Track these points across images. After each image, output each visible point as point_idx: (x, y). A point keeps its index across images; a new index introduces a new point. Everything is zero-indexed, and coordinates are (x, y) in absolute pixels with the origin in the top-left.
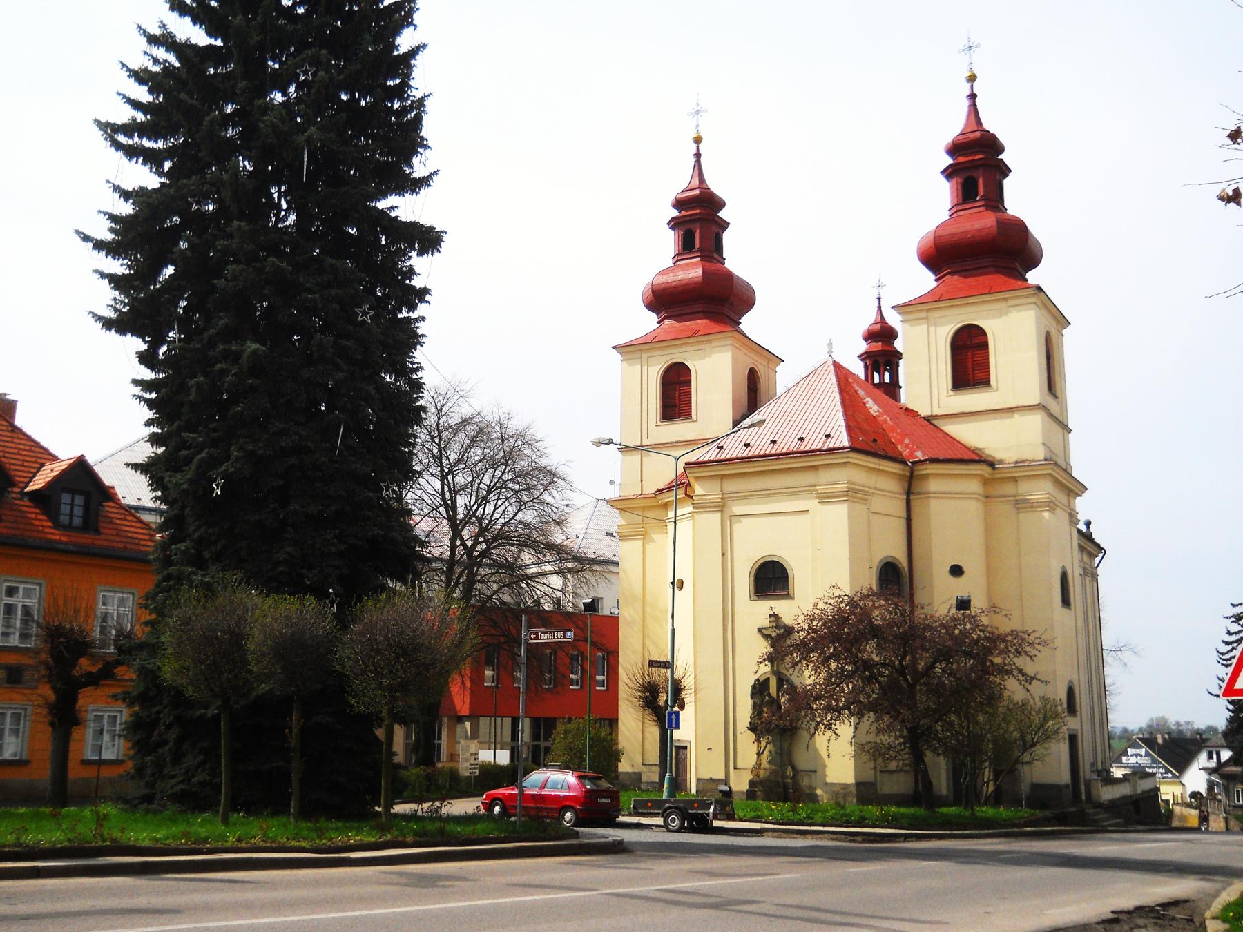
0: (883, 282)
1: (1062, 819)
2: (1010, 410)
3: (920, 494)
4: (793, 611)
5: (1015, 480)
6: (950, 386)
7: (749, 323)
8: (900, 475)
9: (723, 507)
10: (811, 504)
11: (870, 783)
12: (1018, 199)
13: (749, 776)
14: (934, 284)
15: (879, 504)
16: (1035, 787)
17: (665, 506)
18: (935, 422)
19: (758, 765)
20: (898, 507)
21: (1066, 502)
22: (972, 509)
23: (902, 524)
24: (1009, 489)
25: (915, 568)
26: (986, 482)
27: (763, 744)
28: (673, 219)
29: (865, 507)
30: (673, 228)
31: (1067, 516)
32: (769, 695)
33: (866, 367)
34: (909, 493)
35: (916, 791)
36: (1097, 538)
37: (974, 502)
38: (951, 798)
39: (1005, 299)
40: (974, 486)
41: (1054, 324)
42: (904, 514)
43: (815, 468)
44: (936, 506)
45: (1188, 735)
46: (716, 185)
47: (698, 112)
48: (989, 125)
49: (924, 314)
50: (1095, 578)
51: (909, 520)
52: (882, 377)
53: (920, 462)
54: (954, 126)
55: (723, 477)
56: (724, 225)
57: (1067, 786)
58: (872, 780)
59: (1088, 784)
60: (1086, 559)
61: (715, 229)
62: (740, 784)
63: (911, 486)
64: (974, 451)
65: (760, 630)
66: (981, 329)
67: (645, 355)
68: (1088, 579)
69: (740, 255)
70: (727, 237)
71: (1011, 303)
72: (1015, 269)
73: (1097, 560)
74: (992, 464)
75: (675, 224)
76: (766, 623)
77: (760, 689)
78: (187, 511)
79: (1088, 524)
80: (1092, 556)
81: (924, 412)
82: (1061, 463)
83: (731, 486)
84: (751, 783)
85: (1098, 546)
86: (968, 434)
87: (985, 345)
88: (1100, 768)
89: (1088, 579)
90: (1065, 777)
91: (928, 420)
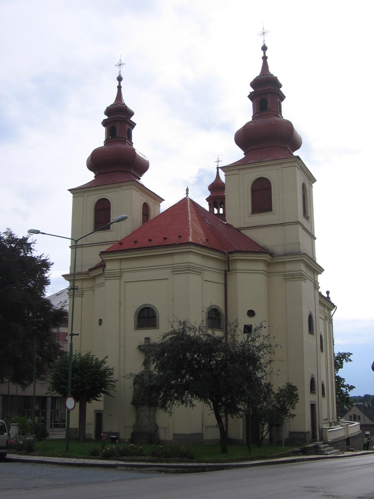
0: (123, 61)
1: (305, 452)
2: (282, 224)
3: (233, 270)
4: (156, 336)
5: (284, 263)
7: (146, 180)
9: (120, 277)
10: (166, 273)
11: (200, 434)
12: (289, 111)
13: (131, 431)
14: (244, 156)
15: (208, 275)
16: (291, 433)
17: (94, 278)
18: (243, 232)
20: (220, 278)
21: (313, 278)
22: (261, 279)
24: (280, 268)
25: (228, 314)
26: (268, 264)
28: (104, 120)
29: (200, 277)
30: (104, 126)
31: (312, 284)
33: (210, 205)
35: (159, 442)
36: (333, 300)
39: (280, 164)
41: (308, 180)
43: (172, 254)
44: (240, 277)
46: (129, 101)
47: (120, 65)
48: (273, 70)
49: (237, 172)
50: (331, 321)
51: (226, 285)
52: (219, 211)
54: (256, 72)
55: (121, 260)
56: (133, 125)
57: (309, 432)
58: (201, 432)
60: (326, 311)
61: (127, 127)
66: (268, 180)
67: (86, 195)
68: (327, 322)
69: (141, 142)
70: (135, 132)
71: (284, 165)
72: (287, 148)
73: (332, 312)
74: (272, 254)
75: (105, 123)
79: (328, 293)
80: (330, 310)
81: (236, 226)
82: (311, 256)
83: (126, 265)
84: (133, 434)
85: (333, 304)
86: (261, 237)
87: (270, 189)
88: (331, 421)
89: (327, 322)
90: (308, 428)
91: (238, 230)
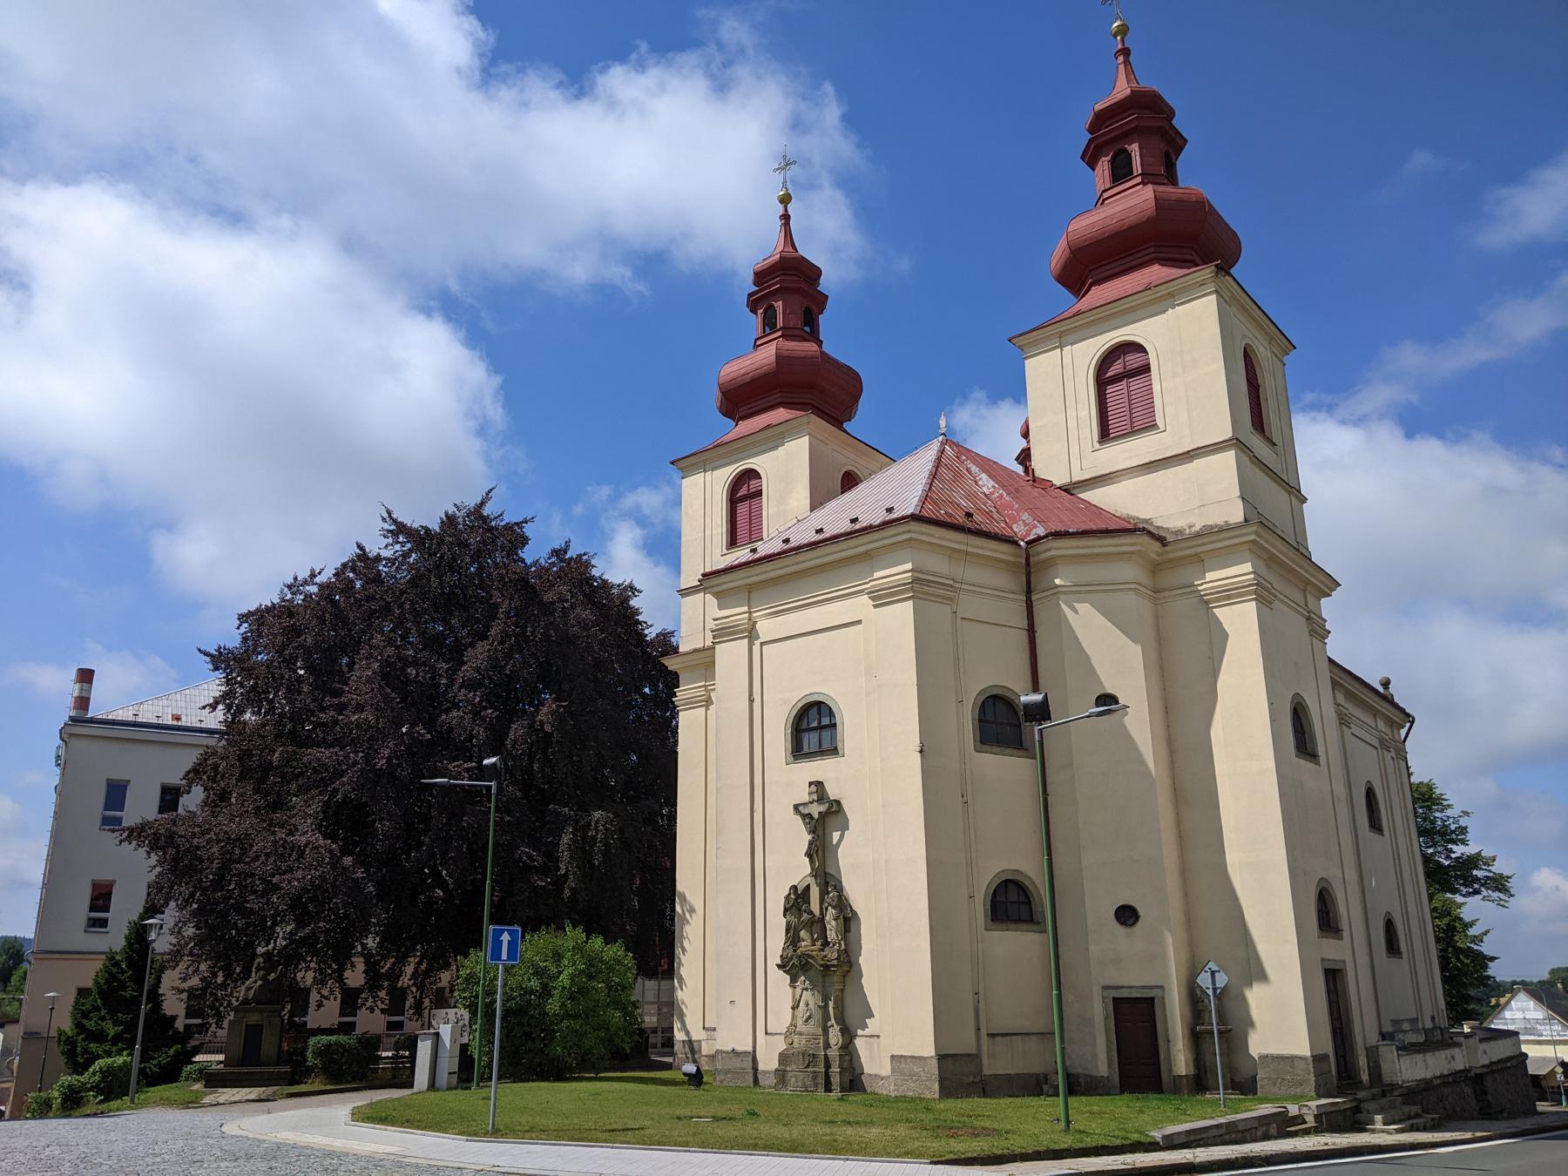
6: (1096, 438)
8: (1014, 564)
10: (860, 606)
19: (792, 1030)
23: (1023, 637)
26: (1156, 568)
27: (798, 990)
32: (811, 913)
34: (1029, 592)
37: (1132, 597)
38: (1116, 1079)
40: (1130, 572)
42: (1025, 624)
45: (580, 272)
53: (1039, 538)
59: (1372, 1053)
62: (768, 1062)
63: (1029, 571)
64: (1126, 520)
65: (796, 807)
73: (1403, 732)
76: (803, 795)
77: (797, 900)
78: (649, 829)
80: (1395, 725)
85: (1403, 711)
86: (1118, 500)
88: (1429, 1025)
